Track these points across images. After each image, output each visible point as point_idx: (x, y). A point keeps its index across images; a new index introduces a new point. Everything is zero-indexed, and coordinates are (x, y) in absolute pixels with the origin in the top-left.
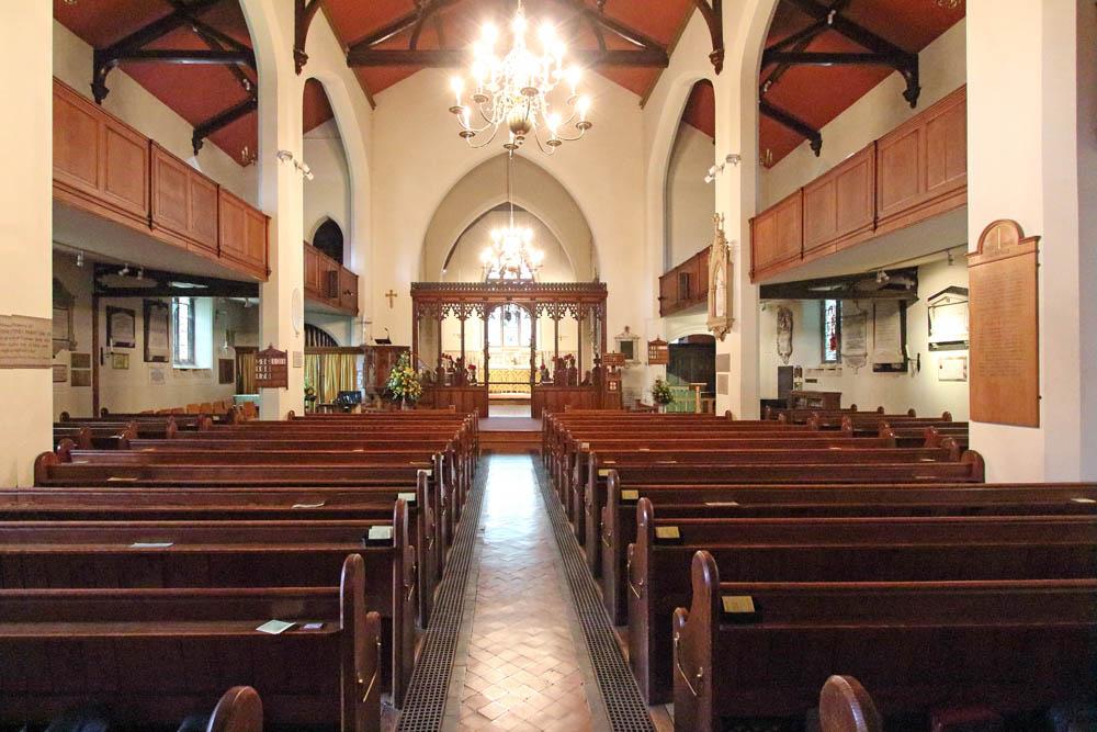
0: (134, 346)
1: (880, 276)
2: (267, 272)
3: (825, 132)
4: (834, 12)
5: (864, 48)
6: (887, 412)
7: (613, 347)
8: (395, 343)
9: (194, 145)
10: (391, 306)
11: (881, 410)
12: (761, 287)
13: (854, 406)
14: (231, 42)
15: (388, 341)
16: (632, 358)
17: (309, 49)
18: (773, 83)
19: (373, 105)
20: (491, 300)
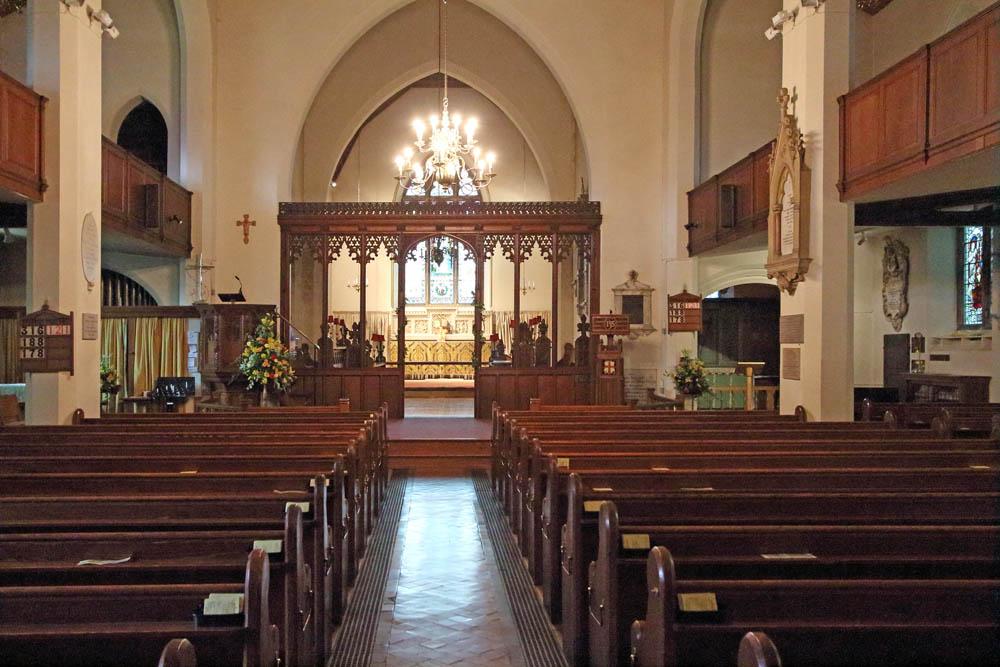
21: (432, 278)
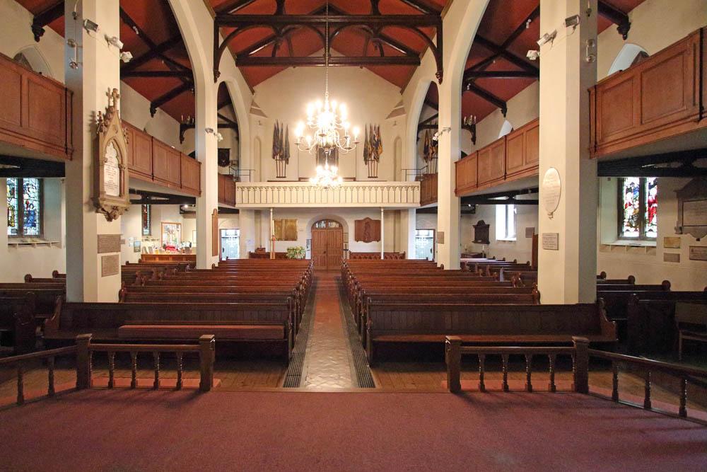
2: (200, 193)
4: (529, 21)
5: (519, 68)
6: (673, 289)
9: (151, 111)
11: (631, 279)
14: (181, 66)
17: (220, 70)
18: (532, 20)
19: (253, 92)
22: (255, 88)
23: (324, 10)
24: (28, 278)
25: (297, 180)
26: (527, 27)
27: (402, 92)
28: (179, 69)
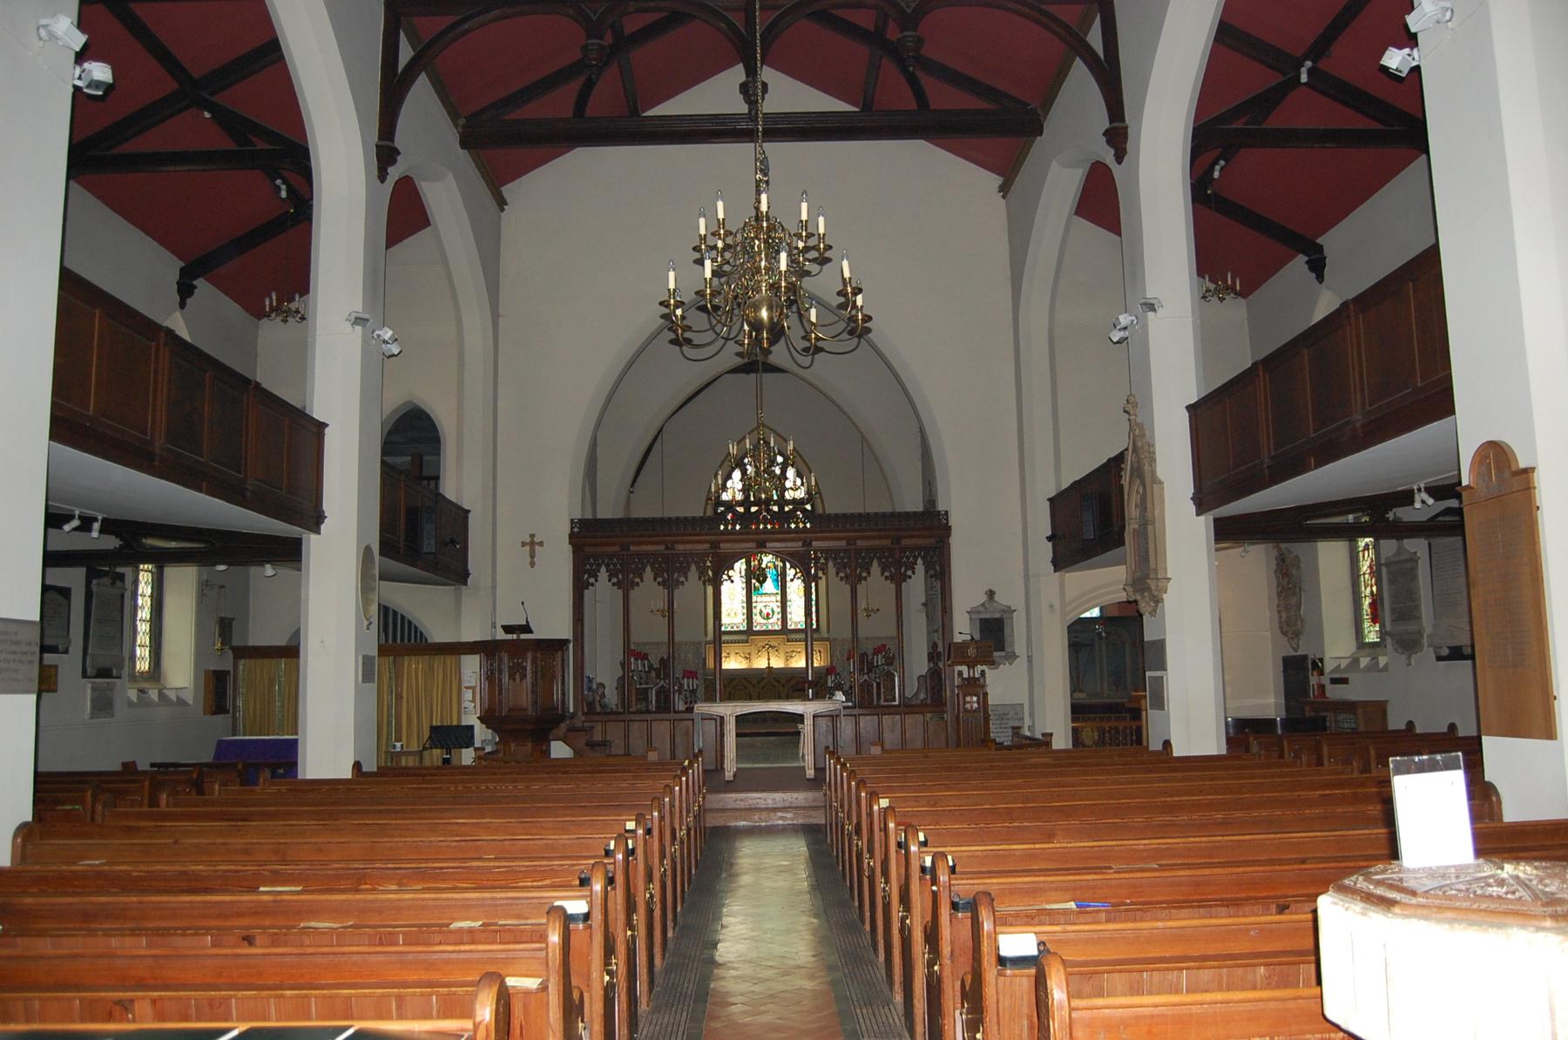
0: (66, 652)
1: (1417, 498)
3: (1331, 242)
4: (1309, 64)
6: (1419, 730)
7: (963, 629)
8: (540, 632)
10: (532, 564)
12: (1216, 520)
13: (1410, 724)
15: (526, 629)
16: (1002, 649)
20: (726, 547)
21: (754, 599)
22: (506, 190)
23: (765, 173)
24: (1528, 471)
25: (1319, 988)
26: (1216, 174)
27: (1004, 189)
28: (261, 145)
